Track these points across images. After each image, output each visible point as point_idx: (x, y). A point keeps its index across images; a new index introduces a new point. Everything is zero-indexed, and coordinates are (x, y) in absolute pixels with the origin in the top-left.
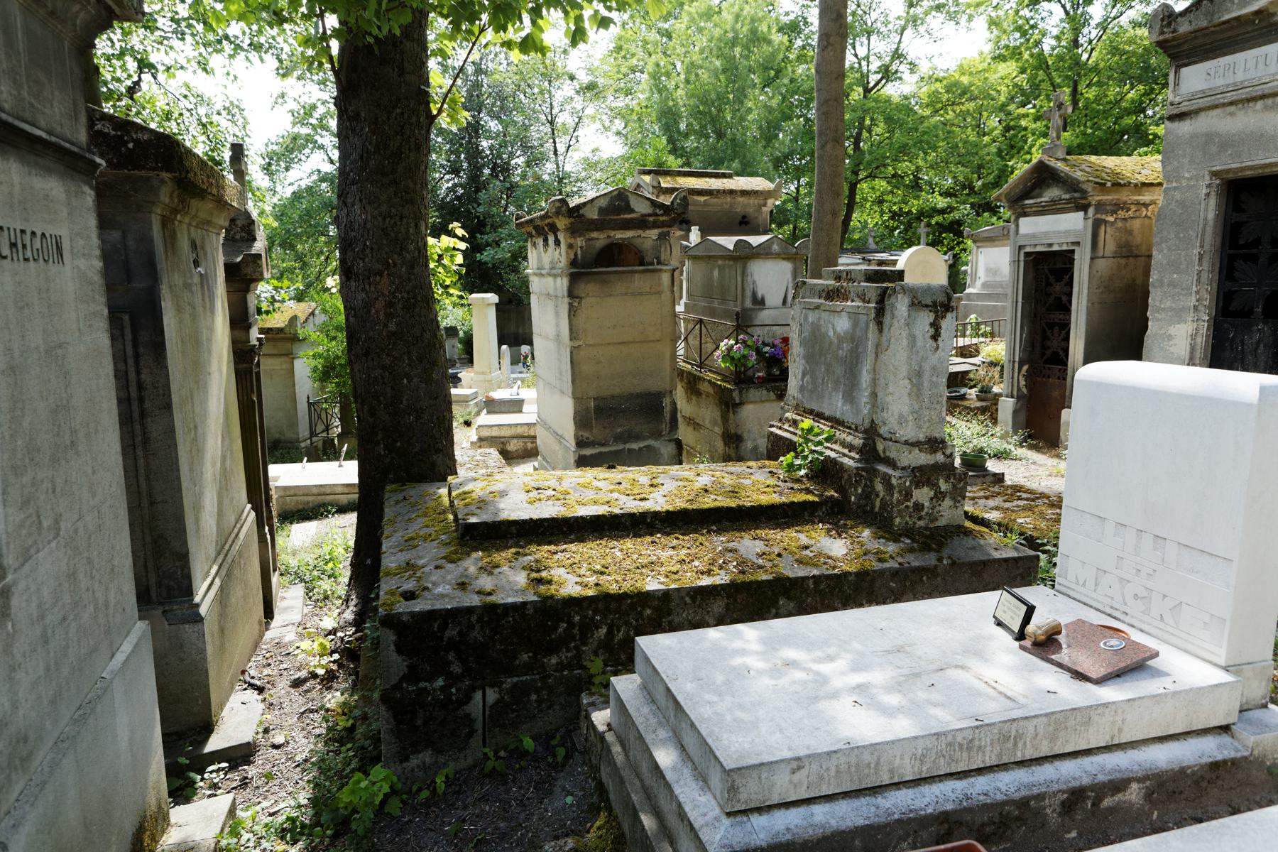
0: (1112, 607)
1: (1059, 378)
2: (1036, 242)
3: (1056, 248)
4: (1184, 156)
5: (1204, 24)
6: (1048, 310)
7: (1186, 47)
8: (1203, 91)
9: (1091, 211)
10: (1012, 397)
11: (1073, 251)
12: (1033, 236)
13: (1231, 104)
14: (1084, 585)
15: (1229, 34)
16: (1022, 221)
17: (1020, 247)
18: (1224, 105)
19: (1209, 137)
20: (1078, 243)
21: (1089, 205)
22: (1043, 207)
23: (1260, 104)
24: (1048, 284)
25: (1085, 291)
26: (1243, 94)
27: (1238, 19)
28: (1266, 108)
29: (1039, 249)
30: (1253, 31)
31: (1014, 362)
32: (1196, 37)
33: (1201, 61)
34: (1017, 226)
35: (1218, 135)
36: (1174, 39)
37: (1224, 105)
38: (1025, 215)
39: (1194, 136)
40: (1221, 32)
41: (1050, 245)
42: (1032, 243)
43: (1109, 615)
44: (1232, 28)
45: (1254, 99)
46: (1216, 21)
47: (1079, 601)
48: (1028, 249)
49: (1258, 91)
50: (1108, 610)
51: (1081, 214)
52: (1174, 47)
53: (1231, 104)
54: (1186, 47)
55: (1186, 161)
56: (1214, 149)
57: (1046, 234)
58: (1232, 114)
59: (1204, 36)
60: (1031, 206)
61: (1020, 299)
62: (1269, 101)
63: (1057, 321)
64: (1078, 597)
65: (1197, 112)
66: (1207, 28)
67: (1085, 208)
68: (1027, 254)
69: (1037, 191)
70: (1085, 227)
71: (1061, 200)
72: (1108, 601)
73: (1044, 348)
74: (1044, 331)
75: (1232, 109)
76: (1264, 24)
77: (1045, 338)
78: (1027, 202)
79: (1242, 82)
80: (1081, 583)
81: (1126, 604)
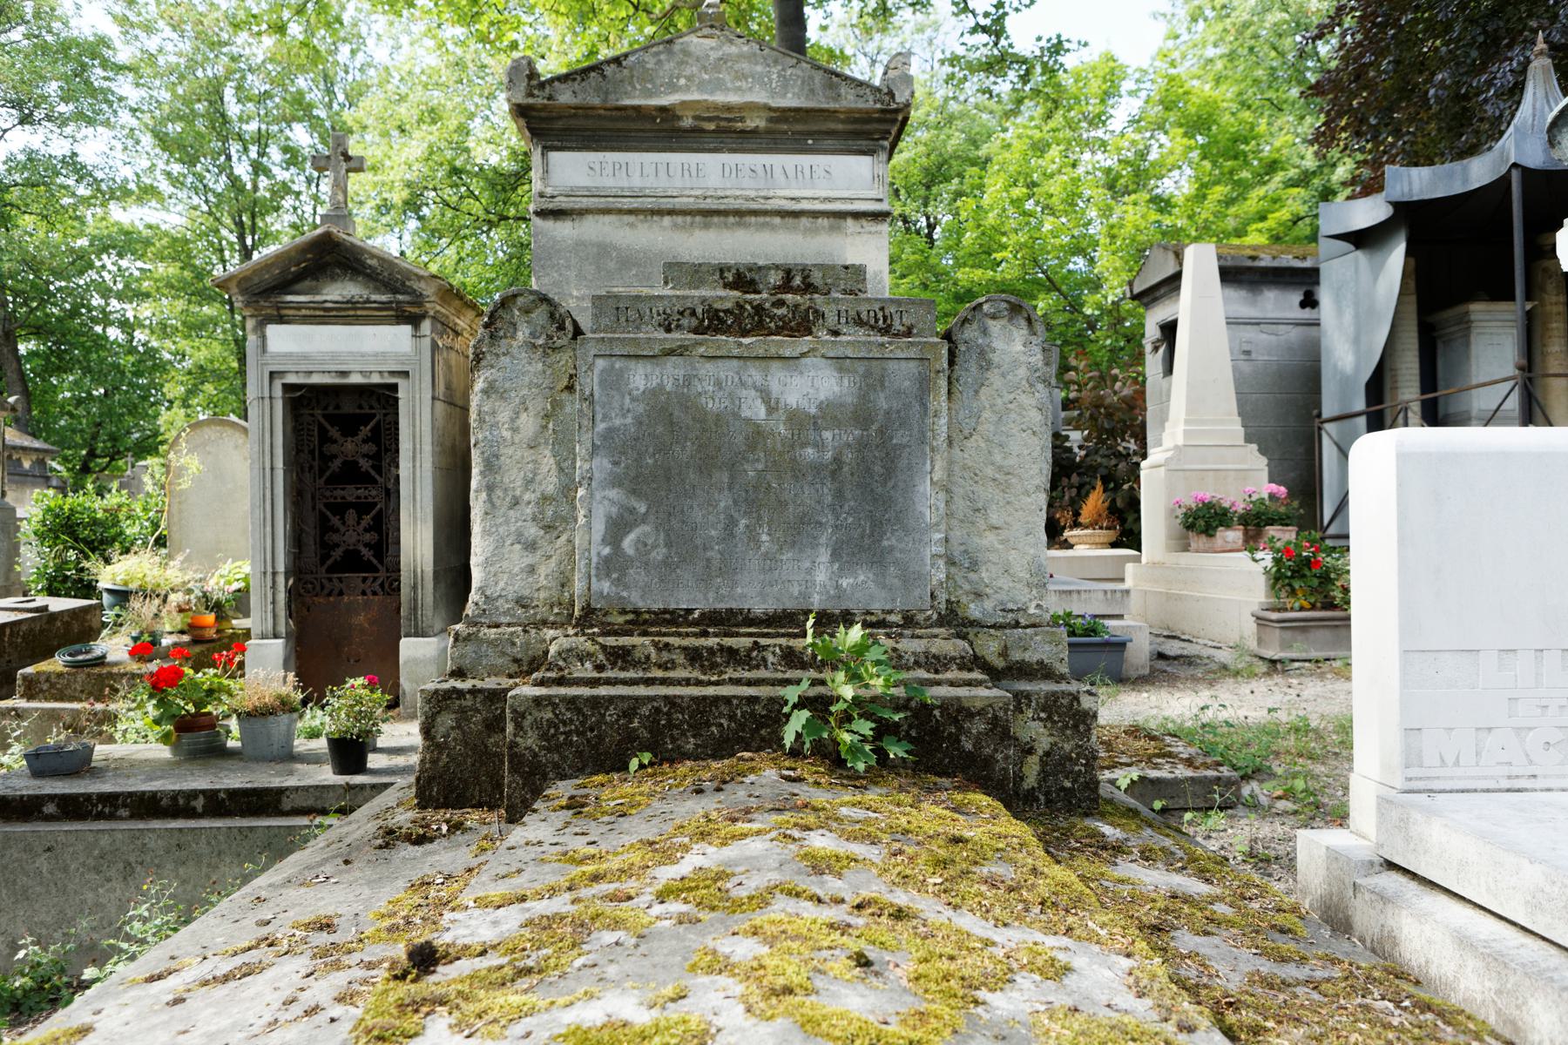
0: (1509, 777)
1: (364, 593)
2: (311, 368)
3: (355, 379)
4: (568, 267)
5: (596, 101)
6: (327, 482)
7: (559, 124)
8: (588, 189)
9: (426, 326)
10: (276, 636)
11: (394, 387)
12: (288, 356)
13: (630, 212)
14: (1457, 763)
15: (620, 125)
16: (272, 330)
17: (272, 373)
18: (620, 212)
19: (603, 250)
20: (406, 374)
21: (423, 316)
22: (326, 309)
23: (667, 220)
24: (325, 438)
25: (427, 448)
26: (648, 203)
27: (637, 109)
28: (675, 226)
29: (316, 379)
30: (651, 131)
31: (274, 574)
32: (575, 115)
33: (579, 149)
34: (263, 338)
35: (615, 248)
36: (545, 107)
37: (620, 212)
38: (281, 320)
39: (580, 244)
40: (612, 119)
41: (344, 374)
42: (304, 368)
43: (1508, 790)
44: (627, 118)
45: (660, 213)
46: (613, 101)
47: (1451, 792)
48: (292, 379)
49: (666, 204)
50: (1505, 784)
51: (406, 330)
52: (542, 119)
53: (630, 212)
54: (559, 124)
55: (572, 274)
56: (612, 265)
57: (335, 356)
58: (631, 225)
59: (586, 117)
60: (299, 306)
61: (279, 464)
62: (679, 219)
63: (350, 499)
64: (1448, 785)
65: (582, 213)
66: (593, 108)
67: (414, 320)
68: (288, 388)
69: (307, 283)
70: (418, 351)
71: (368, 301)
72: (1505, 770)
73: (326, 548)
74: (323, 520)
75: (632, 218)
76: (665, 126)
77: (325, 527)
78: (289, 298)
79: (641, 189)
80: (1450, 760)
81: (1531, 762)
